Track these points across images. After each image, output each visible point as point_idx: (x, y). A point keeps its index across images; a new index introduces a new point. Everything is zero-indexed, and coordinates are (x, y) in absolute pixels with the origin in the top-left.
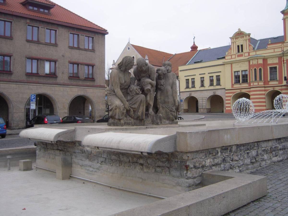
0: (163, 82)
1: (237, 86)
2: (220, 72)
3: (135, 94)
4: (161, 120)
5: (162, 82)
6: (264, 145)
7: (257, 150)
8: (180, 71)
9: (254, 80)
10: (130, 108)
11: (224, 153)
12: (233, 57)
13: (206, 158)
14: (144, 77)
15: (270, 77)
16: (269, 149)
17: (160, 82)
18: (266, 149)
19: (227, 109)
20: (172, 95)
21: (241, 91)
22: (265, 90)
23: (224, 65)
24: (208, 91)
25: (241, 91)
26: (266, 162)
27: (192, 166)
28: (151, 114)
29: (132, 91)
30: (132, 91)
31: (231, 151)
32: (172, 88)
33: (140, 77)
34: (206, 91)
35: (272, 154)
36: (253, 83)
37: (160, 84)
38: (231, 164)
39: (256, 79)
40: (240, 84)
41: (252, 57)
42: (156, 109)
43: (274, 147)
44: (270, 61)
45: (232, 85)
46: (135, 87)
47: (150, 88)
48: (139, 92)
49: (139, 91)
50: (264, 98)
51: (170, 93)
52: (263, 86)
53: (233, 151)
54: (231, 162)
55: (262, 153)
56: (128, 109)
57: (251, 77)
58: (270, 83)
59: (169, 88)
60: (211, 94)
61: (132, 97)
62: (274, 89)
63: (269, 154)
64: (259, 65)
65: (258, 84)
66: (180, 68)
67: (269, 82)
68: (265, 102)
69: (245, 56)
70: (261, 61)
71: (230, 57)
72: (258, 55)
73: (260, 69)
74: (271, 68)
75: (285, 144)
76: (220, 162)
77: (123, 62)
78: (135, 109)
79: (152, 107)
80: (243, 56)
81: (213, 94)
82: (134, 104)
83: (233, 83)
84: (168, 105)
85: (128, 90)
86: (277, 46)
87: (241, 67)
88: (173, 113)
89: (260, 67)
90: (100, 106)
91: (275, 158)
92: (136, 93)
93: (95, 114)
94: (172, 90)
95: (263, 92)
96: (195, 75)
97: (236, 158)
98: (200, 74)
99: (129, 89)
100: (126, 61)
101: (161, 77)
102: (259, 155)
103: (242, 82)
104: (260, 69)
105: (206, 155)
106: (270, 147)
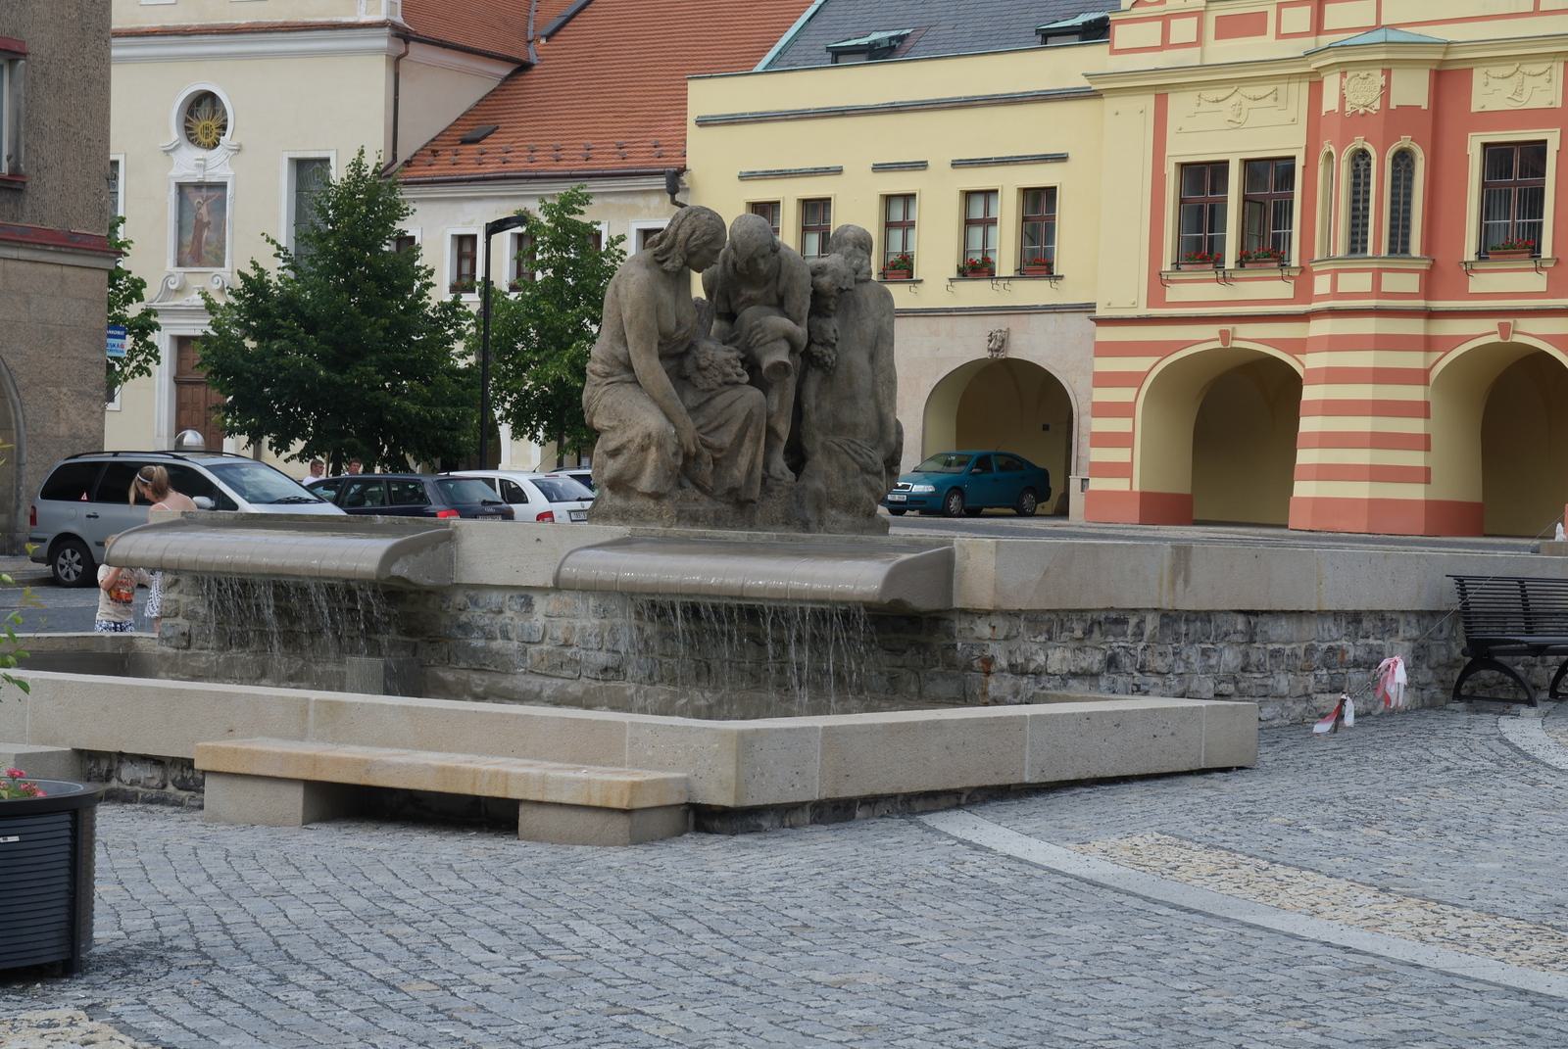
0: (835, 331)
1: (1196, 290)
2: (1062, 158)
3: (720, 385)
4: (819, 509)
5: (832, 326)
6: (1281, 629)
7: (1242, 647)
8: (703, 123)
9: (1341, 247)
10: (700, 446)
11: (1114, 636)
12: (1184, 30)
13: (1050, 643)
14: (751, 302)
15: (1485, 232)
16: (1301, 653)
17: (820, 328)
18: (1288, 652)
19: (1097, 484)
20: (874, 395)
21: (1225, 343)
22: (1429, 344)
23: (1096, 95)
24: (944, 323)
25: (1224, 335)
26: (1283, 707)
27: (1004, 663)
28: (781, 476)
29: (705, 369)
30: (705, 369)
31: (1139, 634)
32: (872, 358)
33: (733, 304)
34: (922, 322)
35: (1316, 675)
36: (1335, 273)
37: (821, 340)
38: (1136, 681)
39: (1357, 242)
40: (1226, 279)
41: (1343, 47)
42: (797, 457)
43: (1325, 646)
44: (1489, 93)
45: (1158, 283)
46: (716, 352)
47: (786, 360)
48: (738, 375)
49: (740, 370)
50: (1423, 410)
51: (863, 382)
52: (1420, 303)
53: (1147, 633)
54: (1136, 674)
55: (1268, 665)
56: (693, 450)
57: (1321, 211)
58: (1479, 283)
59: (859, 358)
60: (969, 345)
61: (708, 396)
62: (1504, 330)
63: (1299, 673)
64: (1395, 118)
65: (1377, 282)
66: (705, 96)
67: (1469, 270)
68: (1425, 443)
69: (1279, 36)
70: (1413, 90)
71: (1151, 33)
72: (1393, 27)
73: (1403, 159)
74: (1497, 157)
75: (1380, 642)
76: (1095, 668)
77: (676, 234)
78: (721, 450)
79: (782, 446)
80: (1263, 32)
81: (987, 355)
82: (717, 428)
83: (1167, 266)
84: (852, 442)
85: (689, 363)
86: (1113, 537)
87: (1239, 126)
88: (873, 480)
89: (1405, 142)
90: (62, 414)
91: (1328, 696)
92: (727, 379)
93: (19, 477)
94: (873, 369)
95: (1415, 360)
96: (839, 171)
97: (1159, 664)
98: (879, 168)
99: (690, 358)
100: (694, 232)
101: (827, 307)
102: (1255, 669)
103: (1241, 263)
104: (1403, 159)
105: (1049, 632)
106: (1303, 646)
